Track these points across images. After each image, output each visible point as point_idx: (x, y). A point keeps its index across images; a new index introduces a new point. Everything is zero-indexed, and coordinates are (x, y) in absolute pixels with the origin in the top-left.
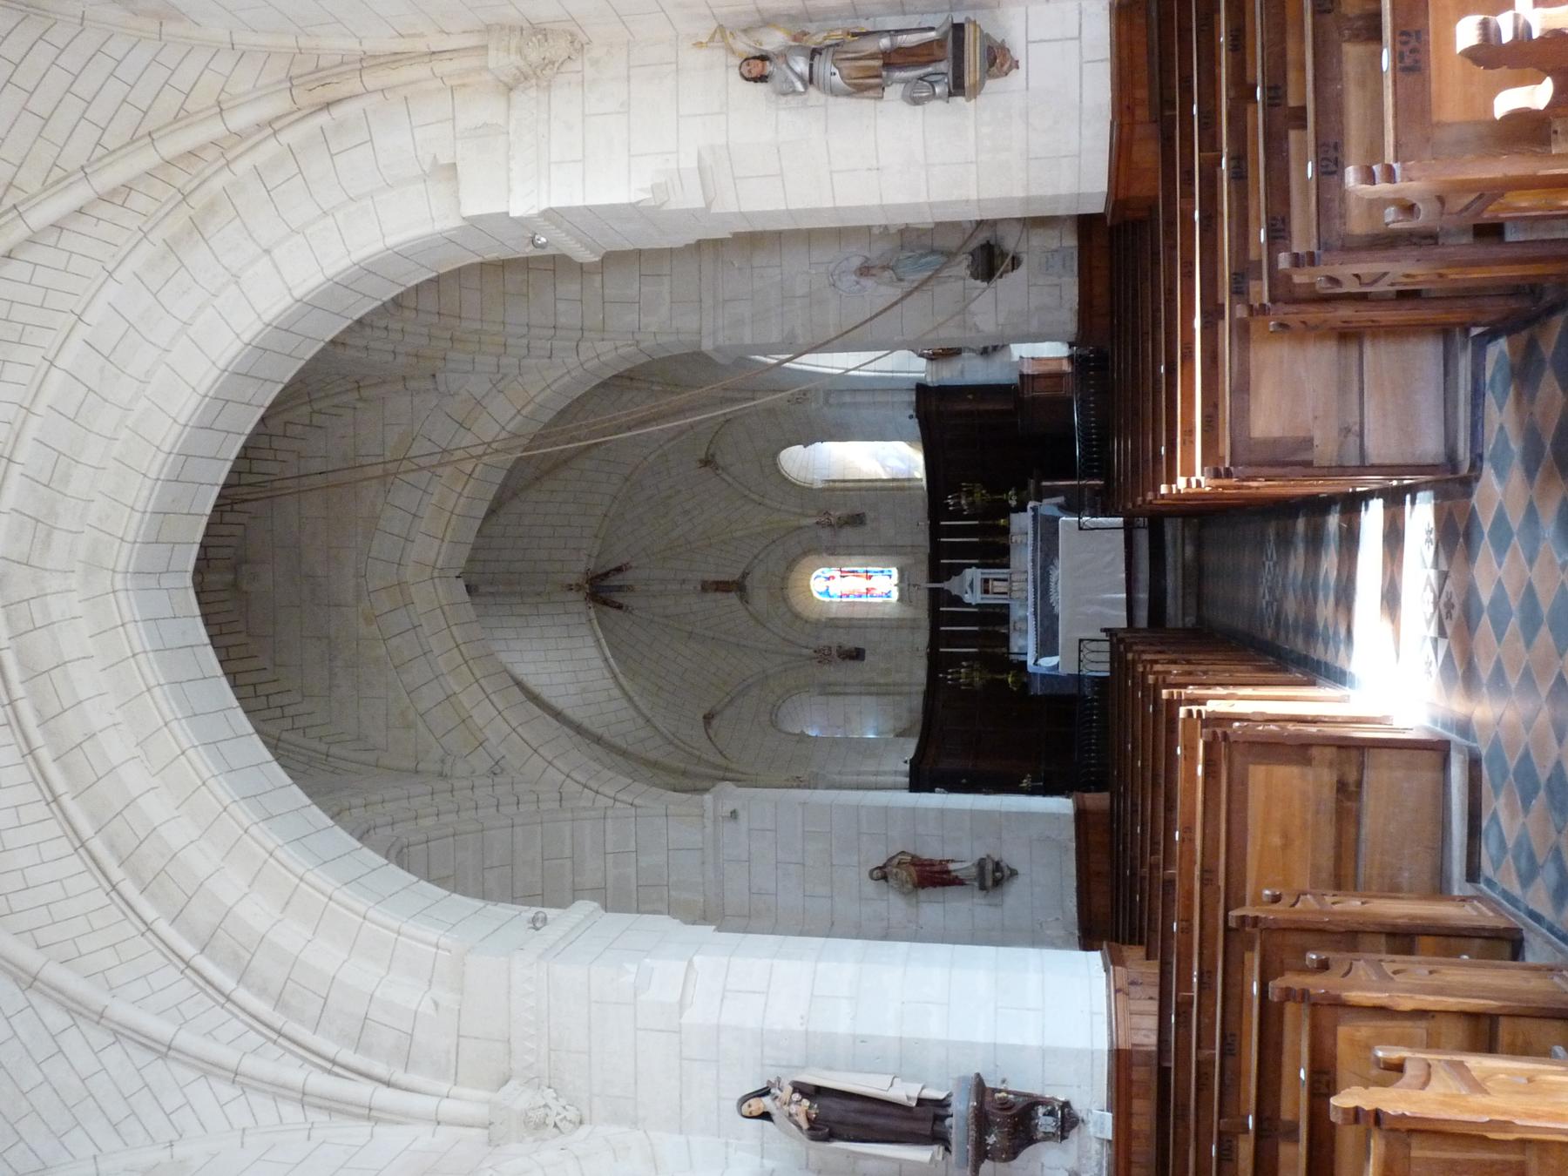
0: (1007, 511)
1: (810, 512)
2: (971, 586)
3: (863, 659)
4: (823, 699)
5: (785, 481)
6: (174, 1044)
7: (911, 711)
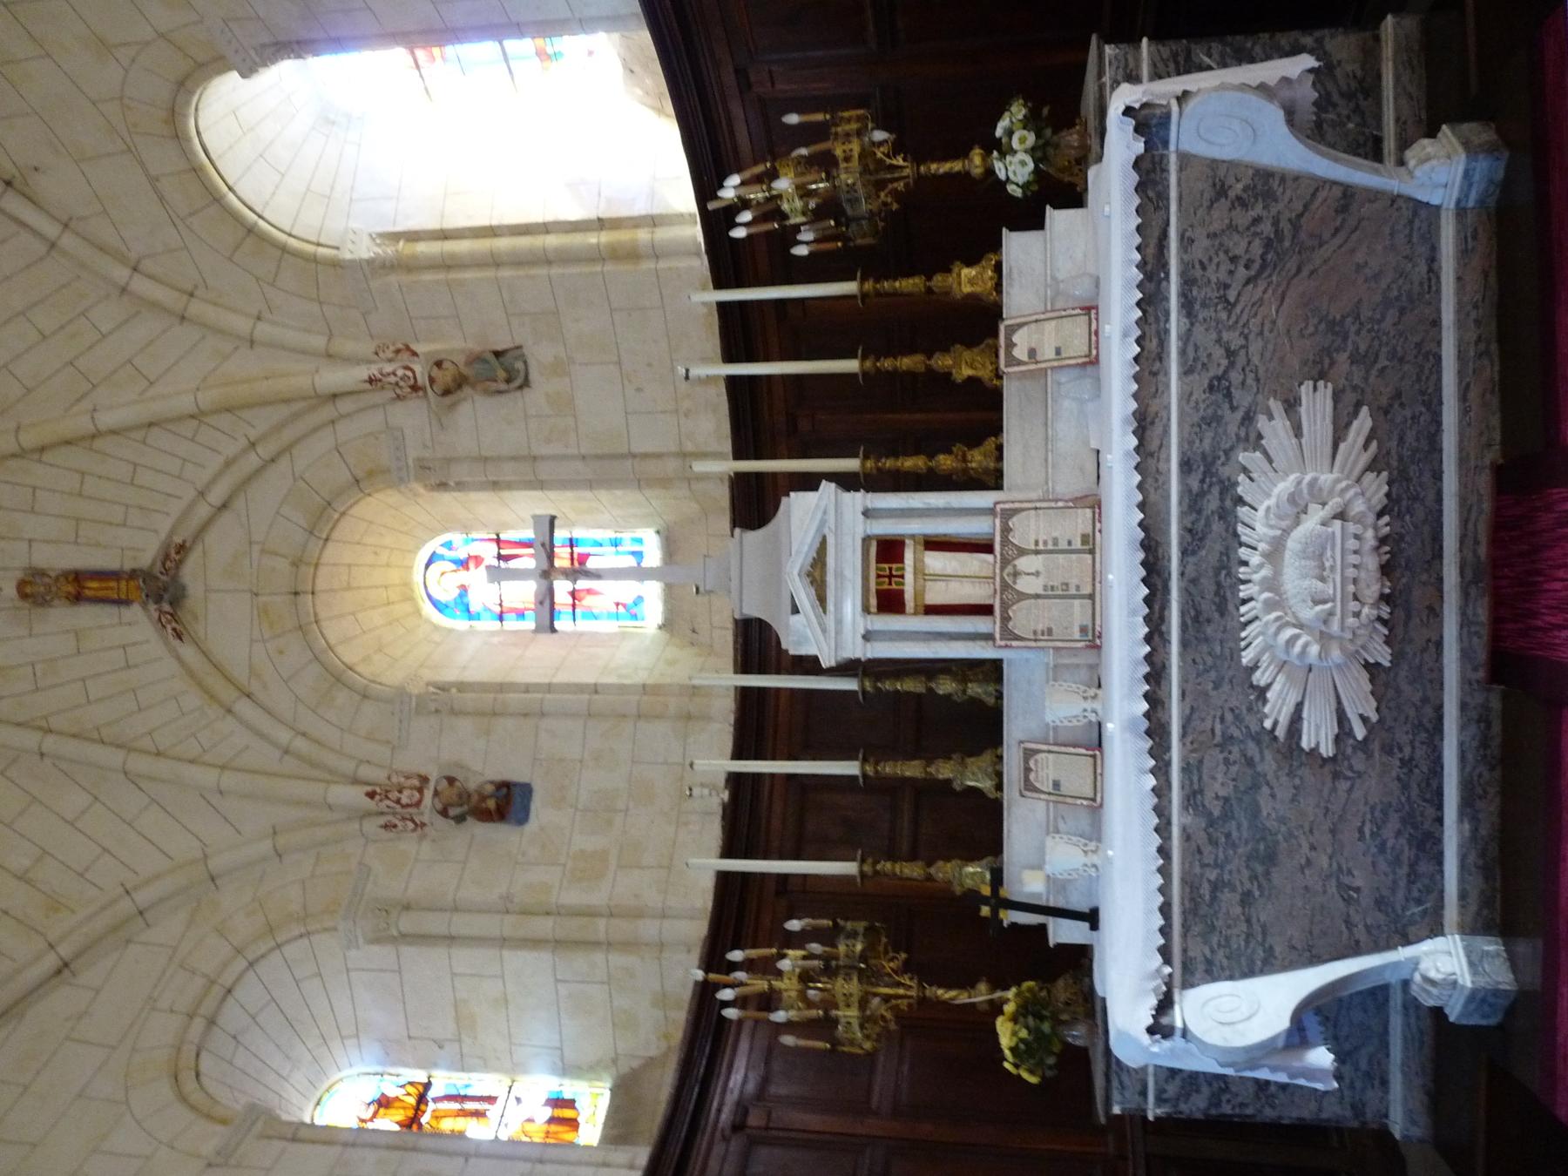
0: (988, 218)
1: (348, 347)
2: (817, 574)
3: (523, 819)
4: (382, 954)
5: (198, 192)
6: (215, 1029)
7: (662, 1000)
